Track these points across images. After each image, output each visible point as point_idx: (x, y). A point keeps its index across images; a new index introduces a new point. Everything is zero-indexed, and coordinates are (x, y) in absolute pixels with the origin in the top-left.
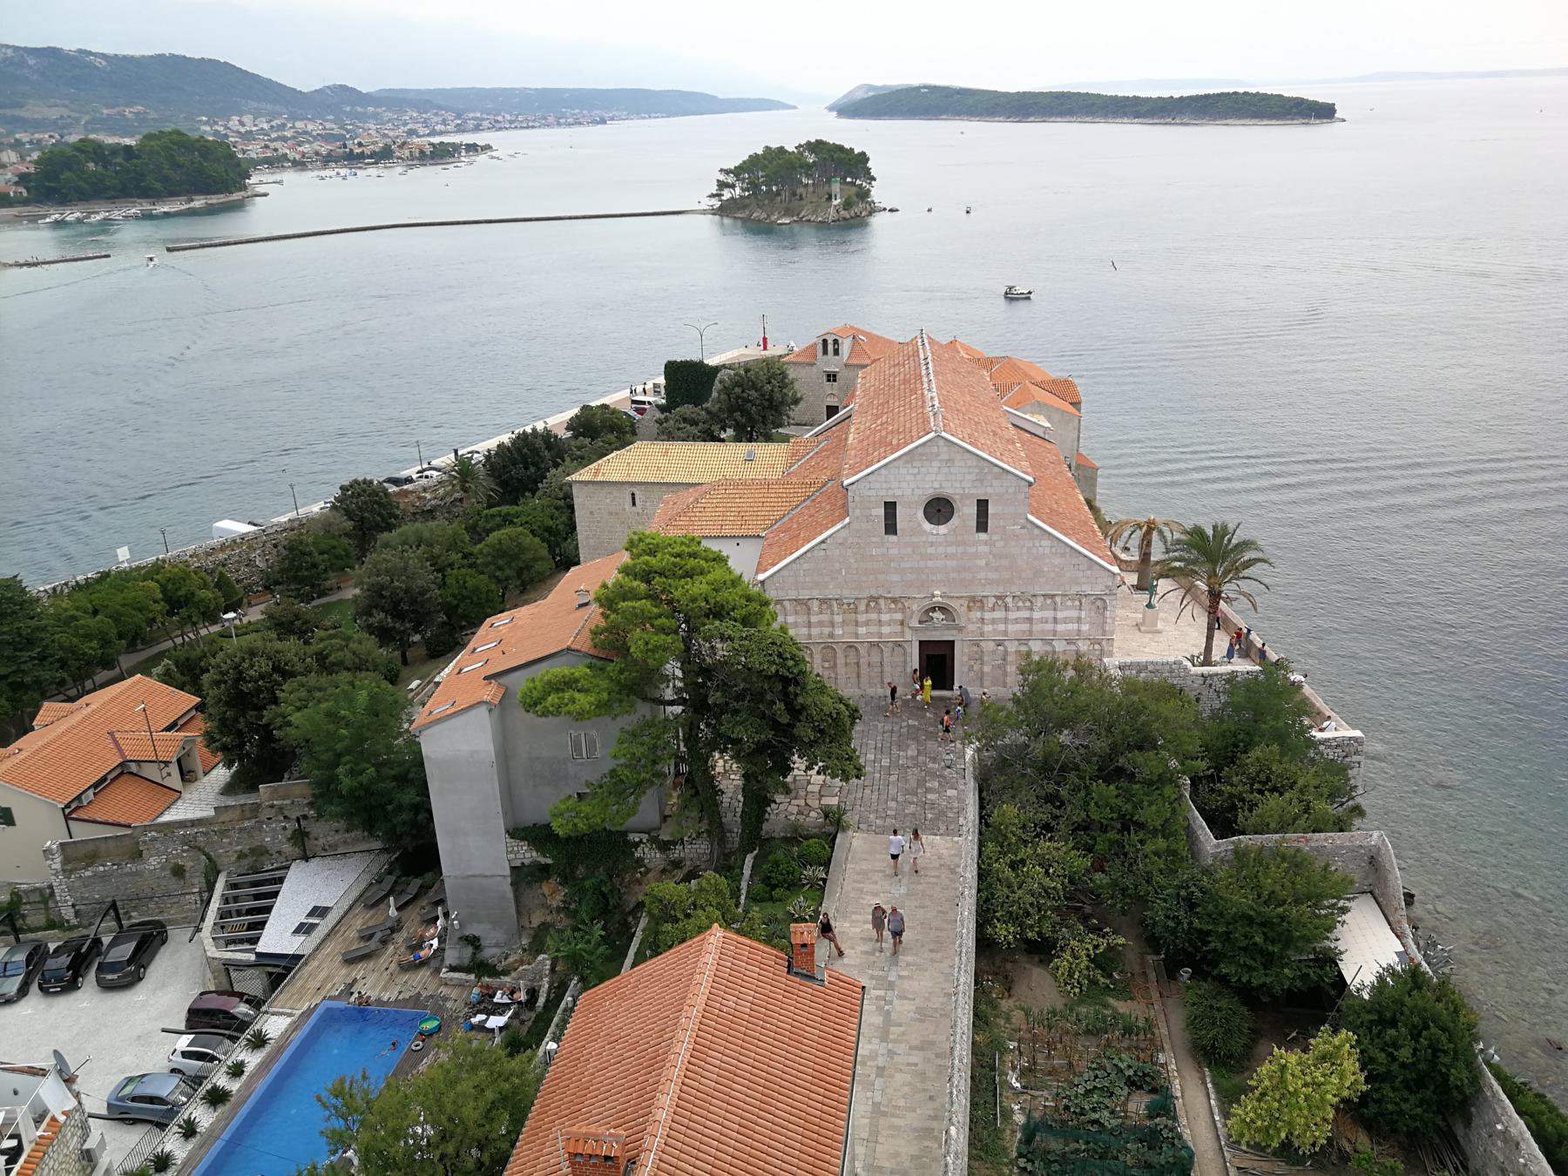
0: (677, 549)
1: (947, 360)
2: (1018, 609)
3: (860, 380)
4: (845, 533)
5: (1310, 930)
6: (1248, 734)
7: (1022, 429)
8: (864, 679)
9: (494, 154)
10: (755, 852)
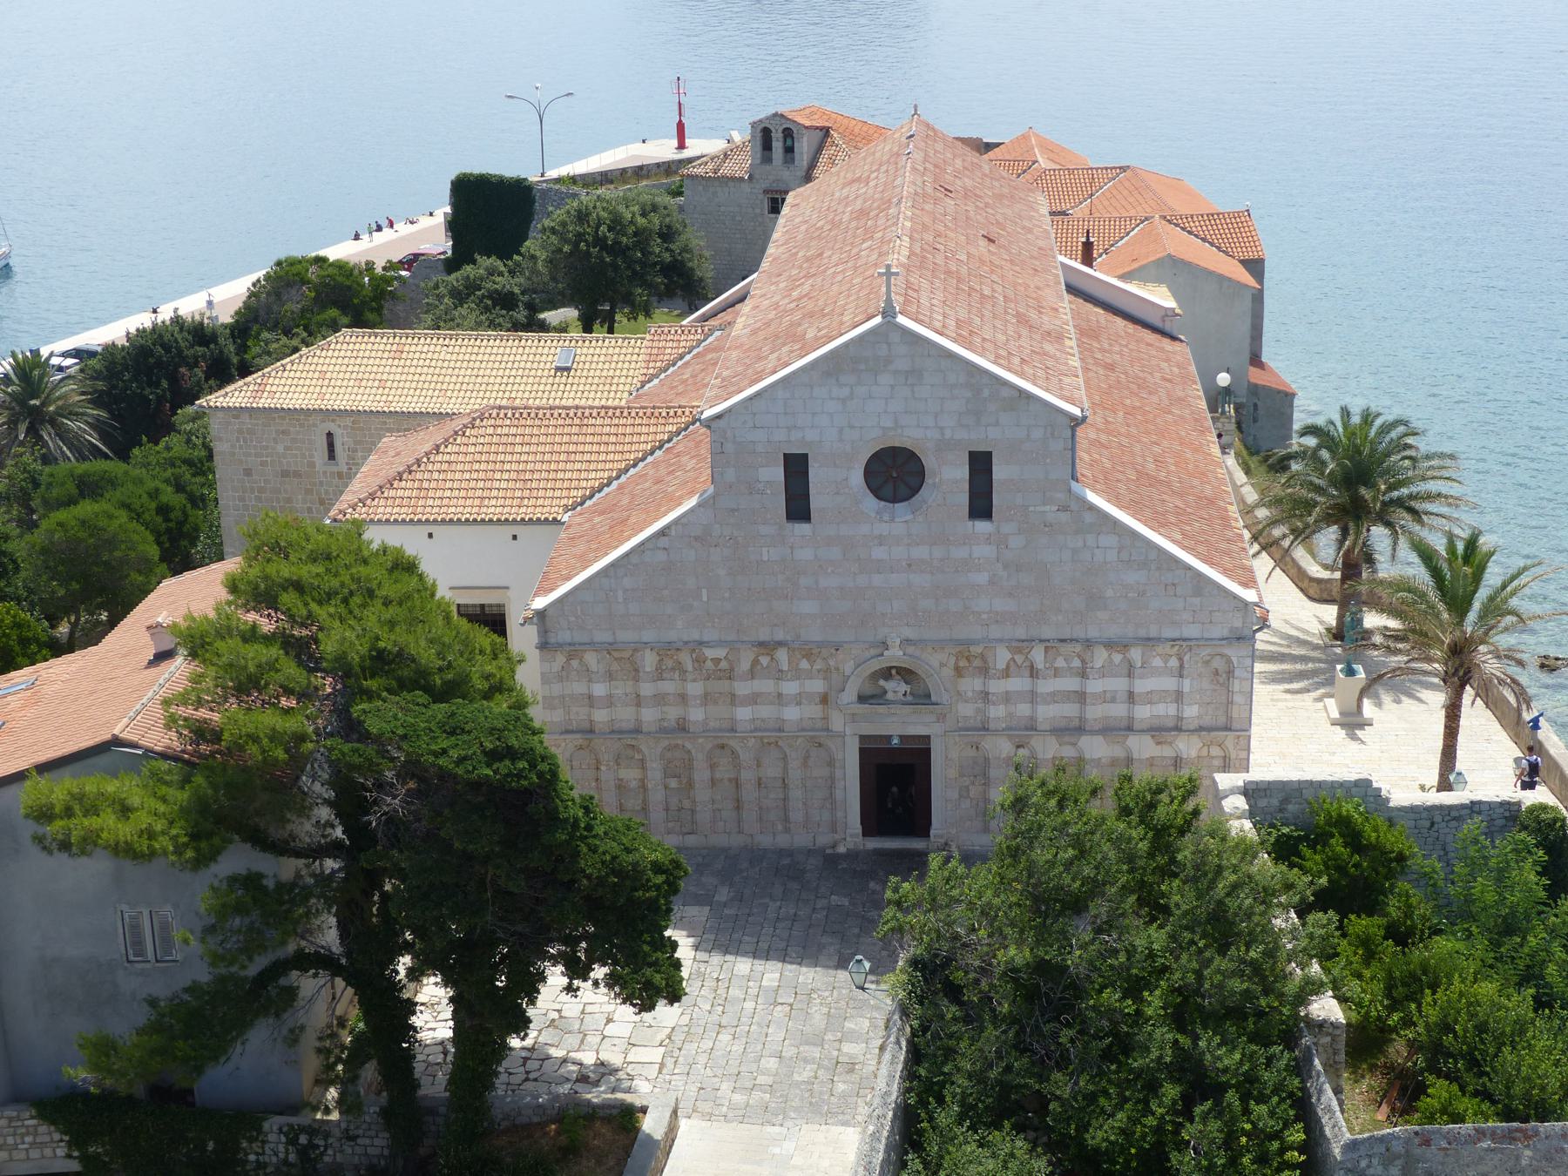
2: (1057, 673)
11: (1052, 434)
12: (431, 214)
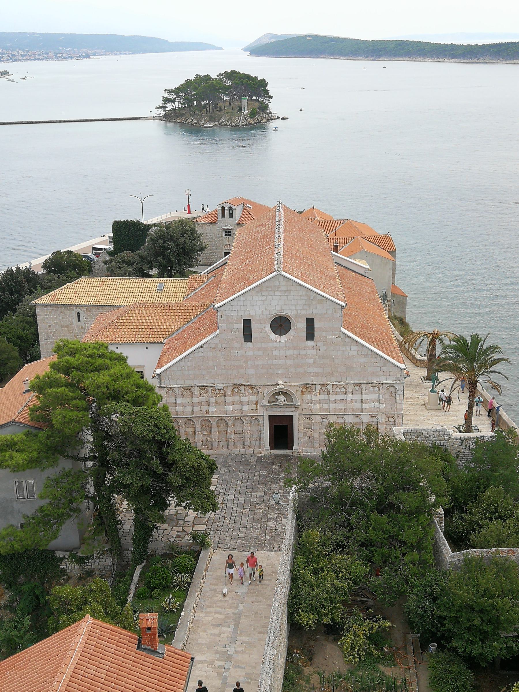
0: (90, 352)
1: (295, 222)
3: (237, 235)
4: (216, 341)
5: (510, 615)
6: (487, 479)
7: (349, 269)
8: (231, 442)
9: (10, 77)
10: (143, 564)
11: (335, 312)
12: (103, 236)
